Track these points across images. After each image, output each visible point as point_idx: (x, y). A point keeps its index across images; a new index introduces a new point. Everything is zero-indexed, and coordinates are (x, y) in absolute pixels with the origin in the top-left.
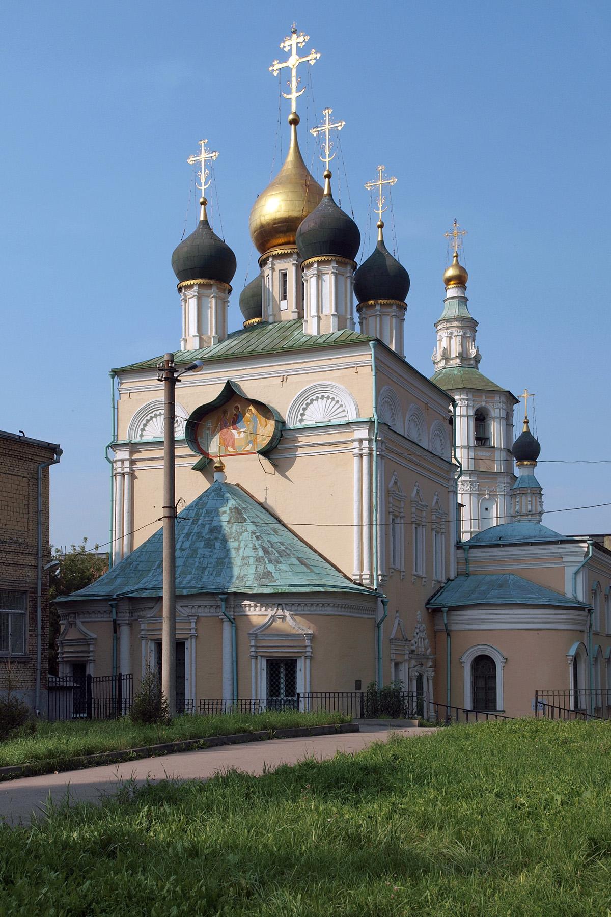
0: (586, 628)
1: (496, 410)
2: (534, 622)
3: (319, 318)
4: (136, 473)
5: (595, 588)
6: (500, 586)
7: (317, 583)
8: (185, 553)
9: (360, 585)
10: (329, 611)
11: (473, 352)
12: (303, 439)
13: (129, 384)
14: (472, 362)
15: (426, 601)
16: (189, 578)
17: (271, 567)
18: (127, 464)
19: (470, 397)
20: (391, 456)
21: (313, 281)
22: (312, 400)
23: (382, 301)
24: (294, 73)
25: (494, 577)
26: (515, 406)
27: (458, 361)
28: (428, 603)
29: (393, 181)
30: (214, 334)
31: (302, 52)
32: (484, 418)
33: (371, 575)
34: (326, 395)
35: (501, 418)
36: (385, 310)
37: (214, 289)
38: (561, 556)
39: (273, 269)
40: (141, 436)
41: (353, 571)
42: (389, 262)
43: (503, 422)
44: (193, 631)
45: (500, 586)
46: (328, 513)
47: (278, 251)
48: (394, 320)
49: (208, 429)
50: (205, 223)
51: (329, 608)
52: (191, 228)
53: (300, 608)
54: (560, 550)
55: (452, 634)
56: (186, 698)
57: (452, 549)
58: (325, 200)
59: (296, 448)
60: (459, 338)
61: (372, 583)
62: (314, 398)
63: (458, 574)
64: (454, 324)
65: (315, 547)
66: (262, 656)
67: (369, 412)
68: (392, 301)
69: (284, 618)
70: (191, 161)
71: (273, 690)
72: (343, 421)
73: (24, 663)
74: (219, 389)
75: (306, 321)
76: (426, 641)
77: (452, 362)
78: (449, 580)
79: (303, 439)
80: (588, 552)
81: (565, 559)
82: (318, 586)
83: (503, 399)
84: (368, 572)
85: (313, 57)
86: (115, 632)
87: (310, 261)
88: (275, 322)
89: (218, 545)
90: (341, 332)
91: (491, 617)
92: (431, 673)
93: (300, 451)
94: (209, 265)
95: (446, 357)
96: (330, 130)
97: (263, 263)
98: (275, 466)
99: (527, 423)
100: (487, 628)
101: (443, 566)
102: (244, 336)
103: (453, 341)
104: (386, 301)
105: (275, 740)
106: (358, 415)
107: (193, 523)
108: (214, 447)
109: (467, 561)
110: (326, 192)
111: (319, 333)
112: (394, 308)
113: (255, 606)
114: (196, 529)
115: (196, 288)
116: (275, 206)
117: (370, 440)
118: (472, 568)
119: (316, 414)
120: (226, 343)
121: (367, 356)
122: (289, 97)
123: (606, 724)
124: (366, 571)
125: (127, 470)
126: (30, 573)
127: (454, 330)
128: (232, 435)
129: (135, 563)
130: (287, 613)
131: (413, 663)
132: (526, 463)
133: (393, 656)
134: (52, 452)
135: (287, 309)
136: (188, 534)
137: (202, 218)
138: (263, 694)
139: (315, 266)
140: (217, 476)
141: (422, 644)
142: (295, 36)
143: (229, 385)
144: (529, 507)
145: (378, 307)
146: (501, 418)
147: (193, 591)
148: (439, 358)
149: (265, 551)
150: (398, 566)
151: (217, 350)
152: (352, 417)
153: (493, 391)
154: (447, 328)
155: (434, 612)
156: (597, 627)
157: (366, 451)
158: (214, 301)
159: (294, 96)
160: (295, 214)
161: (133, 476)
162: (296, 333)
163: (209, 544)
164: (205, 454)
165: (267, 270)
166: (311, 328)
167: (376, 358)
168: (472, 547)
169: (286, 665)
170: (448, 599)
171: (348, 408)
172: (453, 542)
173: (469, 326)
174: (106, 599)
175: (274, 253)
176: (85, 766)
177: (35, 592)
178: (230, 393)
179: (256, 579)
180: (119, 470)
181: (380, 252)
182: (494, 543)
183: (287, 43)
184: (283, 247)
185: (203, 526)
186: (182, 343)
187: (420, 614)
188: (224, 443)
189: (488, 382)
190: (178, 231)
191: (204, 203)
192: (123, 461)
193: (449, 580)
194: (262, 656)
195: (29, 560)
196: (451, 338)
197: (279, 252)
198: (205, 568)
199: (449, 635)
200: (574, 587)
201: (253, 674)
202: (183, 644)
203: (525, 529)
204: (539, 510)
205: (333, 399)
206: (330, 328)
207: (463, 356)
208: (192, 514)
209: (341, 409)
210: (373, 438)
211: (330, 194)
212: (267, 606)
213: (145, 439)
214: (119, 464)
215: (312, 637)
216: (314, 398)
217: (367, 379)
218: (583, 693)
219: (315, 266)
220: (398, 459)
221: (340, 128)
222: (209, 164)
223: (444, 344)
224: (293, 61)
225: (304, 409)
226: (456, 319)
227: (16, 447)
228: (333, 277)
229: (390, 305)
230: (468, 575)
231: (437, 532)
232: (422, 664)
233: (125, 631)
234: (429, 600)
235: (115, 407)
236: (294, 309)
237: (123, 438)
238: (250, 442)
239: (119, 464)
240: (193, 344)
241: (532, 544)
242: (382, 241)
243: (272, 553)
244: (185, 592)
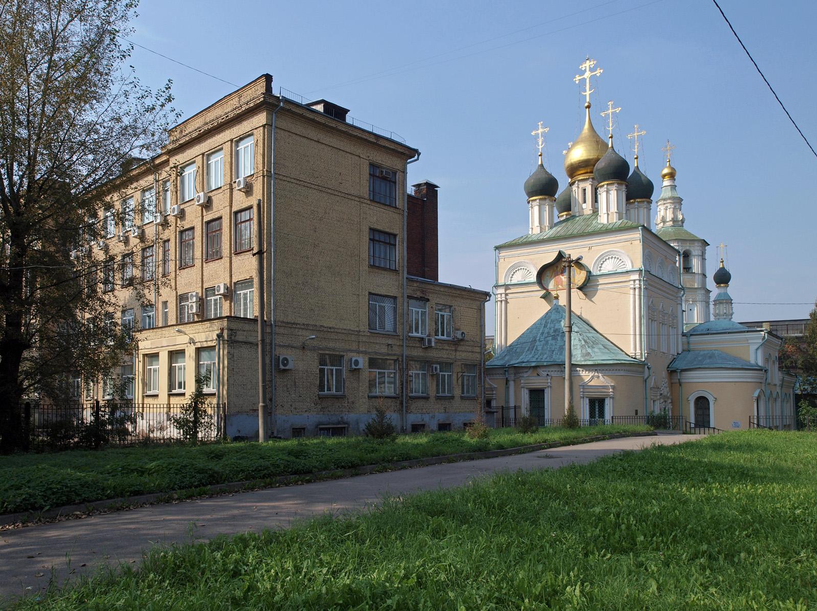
0: (763, 381)
1: (695, 250)
3: (608, 214)
4: (508, 300)
5: (768, 357)
6: (710, 357)
7: (615, 358)
8: (542, 343)
9: (634, 358)
10: (622, 373)
11: (680, 217)
12: (601, 281)
13: (504, 253)
14: (680, 223)
15: (667, 366)
16: (545, 356)
17: (589, 350)
18: (503, 295)
19: (680, 244)
20: (650, 287)
21: (604, 194)
22: (606, 259)
23: (639, 200)
24: (588, 81)
25: (705, 352)
26: (707, 248)
27: (671, 223)
28: (668, 367)
29: (643, 133)
30: (547, 224)
31: (591, 70)
32: (688, 256)
33: (641, 353)
34: (614, 256)
35: (698, 255)
36: (640, 205)
37: (547, 201)
39: (578, 187)
40: (511, 280)
41: (631, 351)
42: (643, 178)
43: (700, 258)
44: (549, 384)
45: (710, 357)
46: (617, 321)
47: (581, 178)
48: (645, 210)
50: (542, 165)
51: (622, 372)
52: (534, 169)
53: (607, 372)
55: (683, 385)
56: (546, 417)
57: (680, 336)
58: (610, 150)
59: (598, 285)
60: (672, 210)
61: (642, 358)
62: (607, 258)
63: (683, 350)
64: (669, 201)
65: (608, 338)
67: (639, 264)
68: (644, 200)
69: (598, 377)
70: (533, 133)
71: (592, 415)
72: (624, 270)
75: (600, 216)
76: (668, 388)
77: (667, 224)
78: (678, 354)
79: (601, 281)
80: (764, 337)
81: (749, 342)
82: (616, 360)
83: (700, 244)
84: (640, 352)
85: (598, 72)
86: (507, 384)
87: (602, 184)
88: (579, 216)
89: (559, 338)
90: (621, 221)
92: (670, 406)
93: (600, 287)
94: (545, 188)
95: (664, 221)
96: (612, 113)
97: (571, 184)
98: (585, 295)
99: (722, 262)
100: (701, 381)
101: (675, 346)
102: (564, 224)
103: (668, 211)
104: (641, 200)
105: (630, 438)
106: (633, 266)
107: (544, 327)
108: (551, 286)
109: (688, 343)
110: (610, 146)
111: (608, 222)
112: (645, 203)
113: (583, 371)
114: (546, 331)
115: (538, 201)
116: (579, 153)
117: (640, 280)
118: (692, 347)
119: (609, 266)
120: (554, 229)
121: (638, 235)
122: (585, 94)
123: (814, 433)
124: (638, 351)
125: (504, 299)
126: (478, 356)
127: (668, 205)
128: (561, 279)
129: (515, 349)
130: (600, 375)
131: (662, 400)
132: (722, 285)
133: (652, 397)
134: (485, 296)
135: (587, 208)
136: (542, 333)
137: (540, 163)
138: (587, 417)
139: (605, 186)
140: (555, 302)
141: (666, 391)
142: (588, 61)
144: (725, 311)
145: (636, 203)
146: (698, 255)
147: (549, 363)
148: (659, 221)
149: (585, 342)
150: (653, 348)
151: (551, 233)
152: (629, 268)
153: (694, 240)
154: (664, 204)
155: (672, 372)
156: (769, 380)
157: (637, 286)
158: (547, 207)
159: (588, 93)
160: (591, 157)
161: (506, 302)
162: (594, 222)
163: (554, 338)
164: (547, 290)
165: (574, 188)
166: (603, 219)
167: (643, 235)
168: (691, 335)
169: (599, 401)
170: (679, 365)
171: (626, 263)
172: (680, 332)
173: (678, 202)
174: (503, 367)
176: (577, 444)
177: (480, 365)
178: (560, 256)
179: (582, 356)
180: (499, 299)
181: (637, 172)
182: (705, 332)
183: (584, 66)
184: (584, 175)
185: (550, 329)
186: (530, 230)
187: (664, 374)
188: (557, 284)
189: (691, 234)
190: (527, 173)
191: (540, 155)
192: (501, 294)
193: (678, 354)
195: (478, 350)
196: (666, 210)
198: (553, 351)
199: (680, 385)
200: (756, 357)
201: (582, 406)
202: (544, 390)
203: (723, 324)
204: (731, 312)
205: (618, 258)
206: (614, 219)
207: (674, 220)
208: (544, 322)
209: (622, 264)
210: (642, 279)
211: (612, 147)
212: (589, 371)
213: (513, 282)
214: (499, 296)
215: (613, 387)
216: (607, 258)
217: (638, 247)
218: (761, 417)
219: (605, 186)
220: (653, 289)
221: (618, 111)
222: (543, 134)
223: (662, 213)
224: (587, 75)
225: (602, 264)
226: (670, 198)
227: (472, 294)
228: (615, 192)
229: (613, 184)
230: (689, 351)
231: (652, 320)
232: (665, 402)
233: (512, 383)
234: (669, 365)
235: (497, 266)
236: (590, 208)
237: (501, 282)
239: (499, 296)
240: (537, 231)
241: (729, 333)
242: (637, 166)
243: (589, 343)
244: (545, 364)
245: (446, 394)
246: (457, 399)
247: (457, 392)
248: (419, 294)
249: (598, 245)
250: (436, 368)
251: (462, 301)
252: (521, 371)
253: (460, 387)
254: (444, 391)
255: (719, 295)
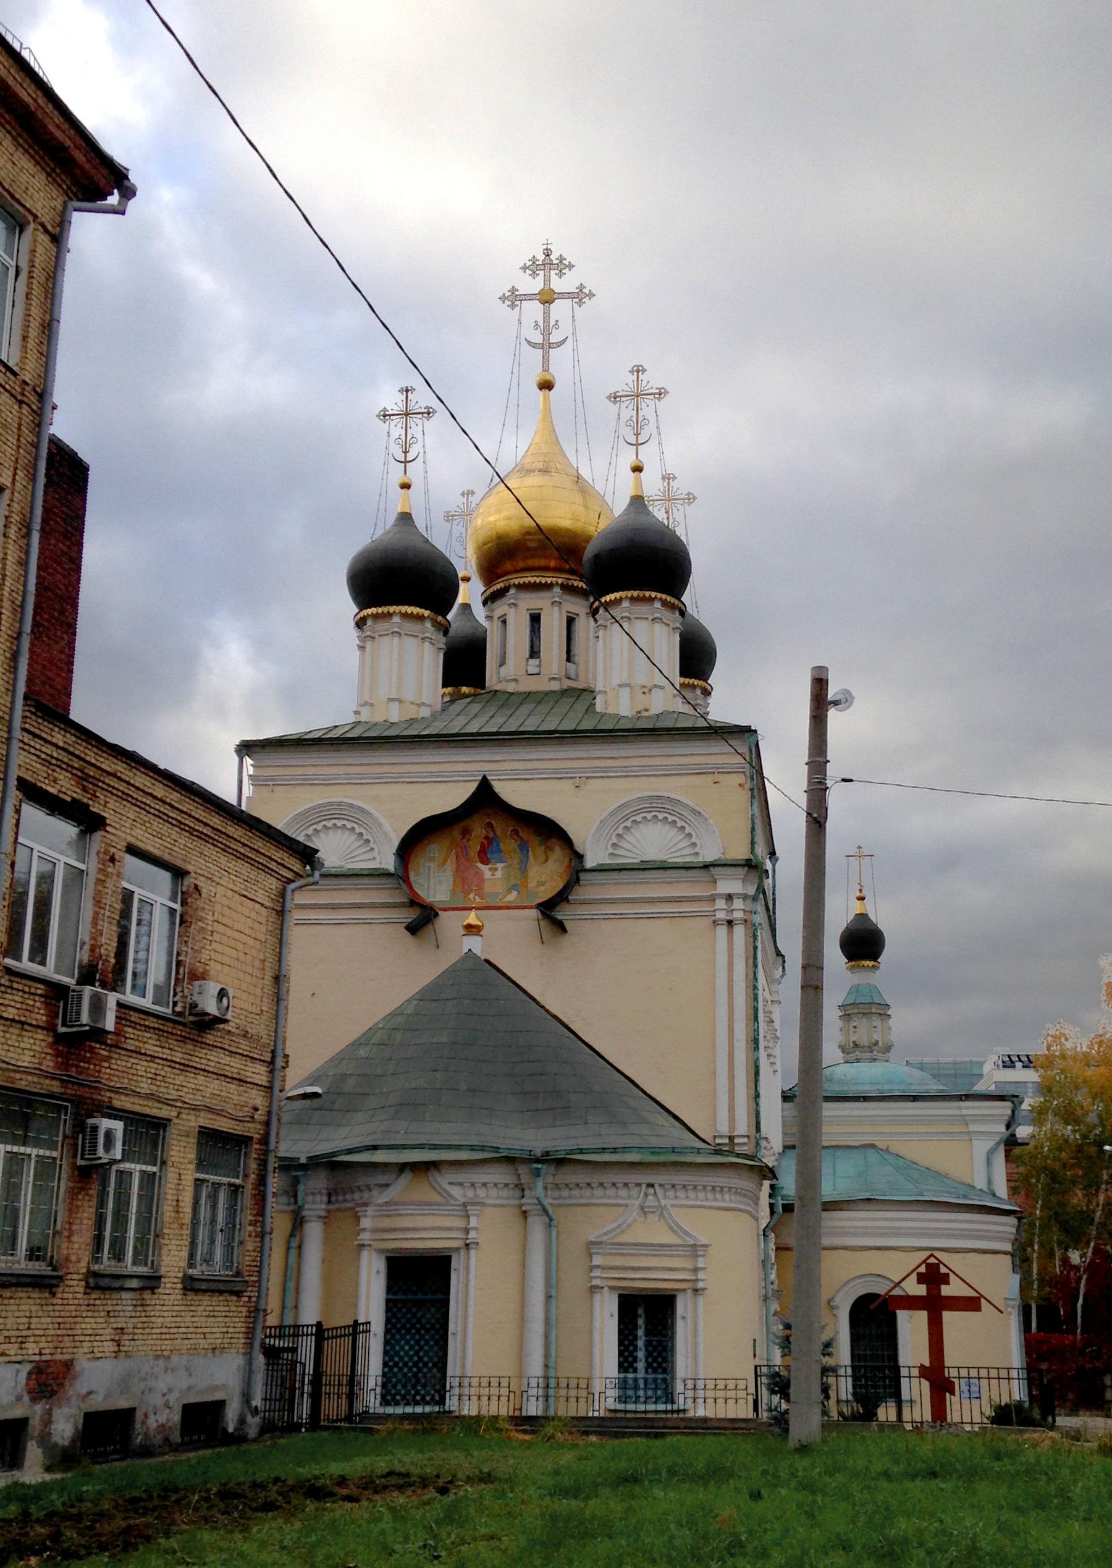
2: (977, 1238)
38: (965, 1120)
49: (432, 859)
54: (964, 1112)
66: (611, 1288)
73: (232, 1293)
74: (471, 788)
81: (973, 1128)
91: (875, 1224)
128: (479, 874)
143: (485, 785)
175: (516, 581)
178: (485, 798)
194: (611, 1288)
195: (258, 1073)
197: (532, 580)
229: (420, 618)
233: (314, 1232)
238: (514, 887)
245: (129, 1265)
246: (171, 1287)
247: (173, 1260)
248: (65, 786)
249: (604, 774)
250: (109, 1135)
251: (223, 860)
252: (362, 1181)
253: (187, 1232)
254: (118, 1255)
255: (856, 989)
